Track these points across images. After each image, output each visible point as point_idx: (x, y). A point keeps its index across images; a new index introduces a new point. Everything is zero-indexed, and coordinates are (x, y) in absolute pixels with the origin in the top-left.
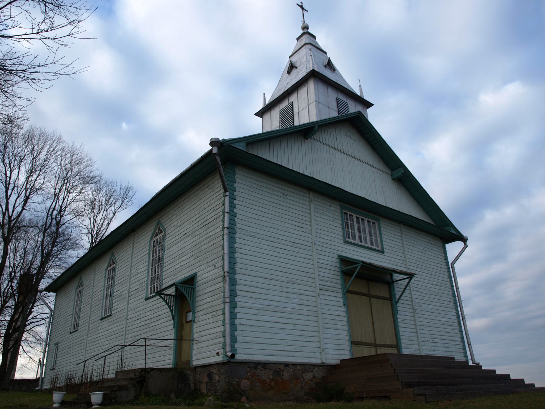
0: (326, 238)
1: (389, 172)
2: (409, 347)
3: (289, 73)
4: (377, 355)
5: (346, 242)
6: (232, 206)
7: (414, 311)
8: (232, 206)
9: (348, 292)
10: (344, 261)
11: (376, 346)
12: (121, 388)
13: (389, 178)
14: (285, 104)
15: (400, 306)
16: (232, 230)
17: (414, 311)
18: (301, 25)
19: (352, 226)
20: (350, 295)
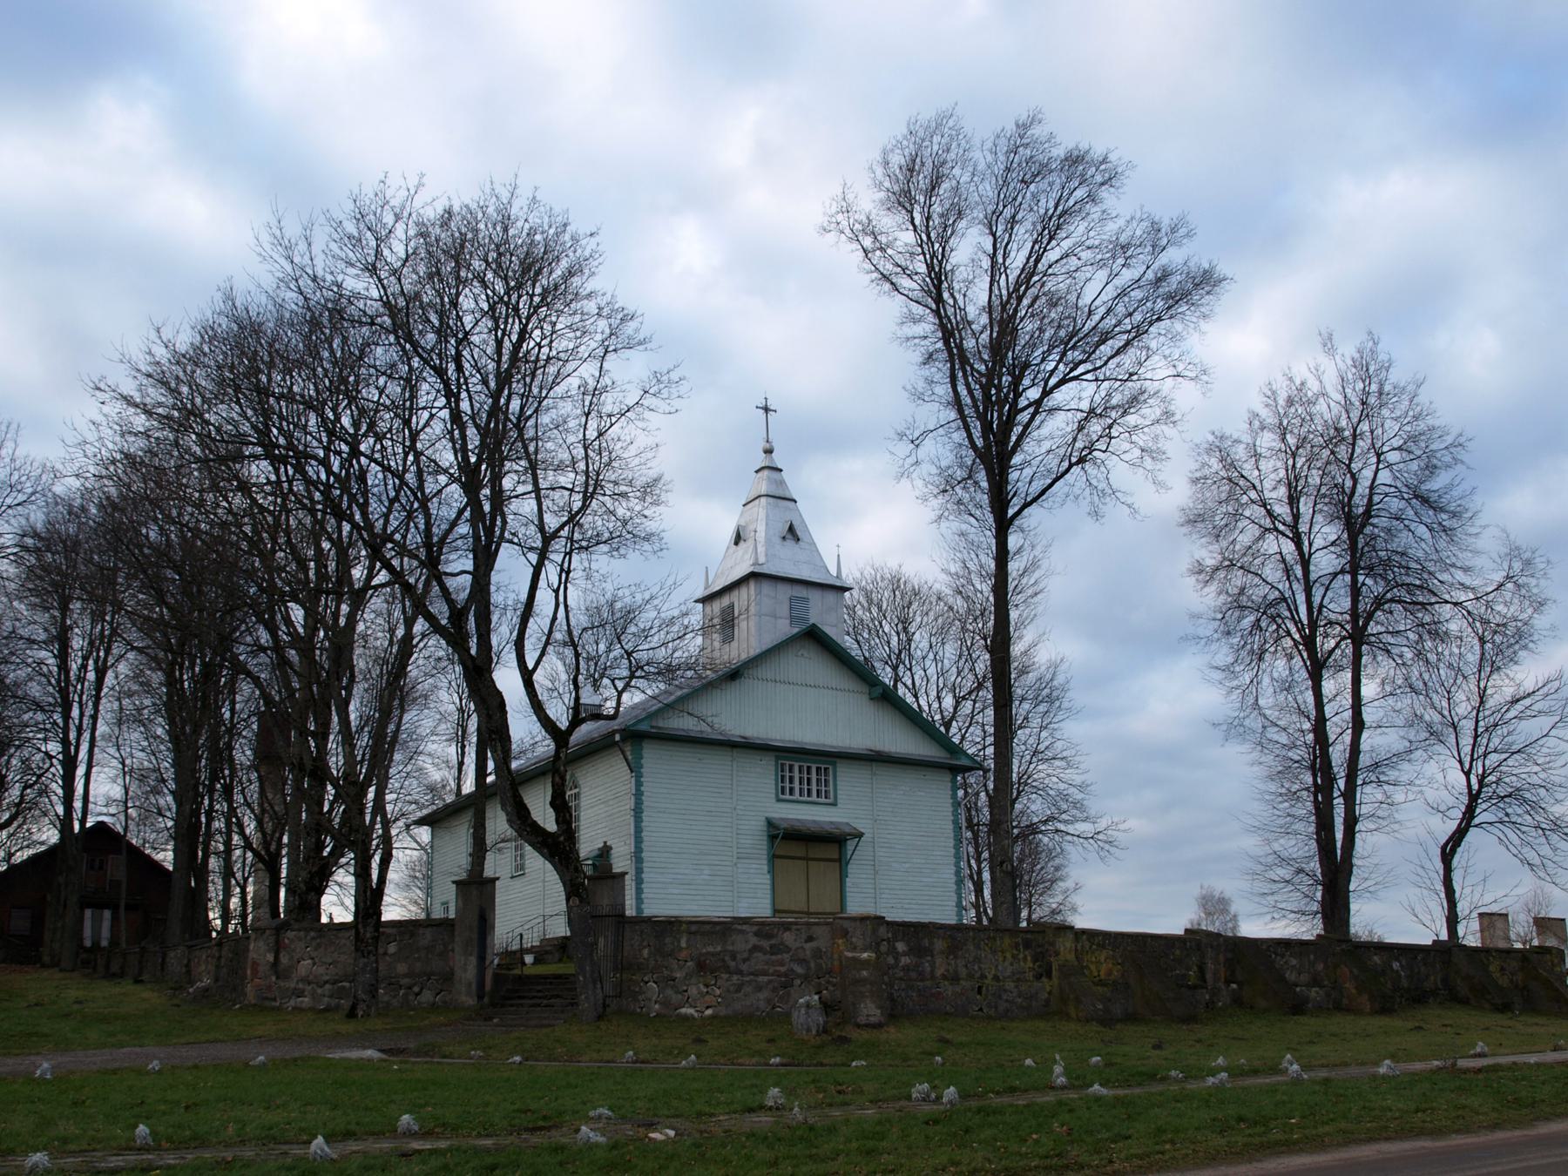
0: (757, 799)
1: (865, 689)
2: (1082, 921)
3: (736, 543)
4: (1339, 974)
5: (779, 800)
6: (639, 784)
7: (876, 873)
8: (639, 784)
9: (773, 858)
10: (770, 823)
11: (808, 913)
12: (547, 952)
13: (865, 698)
14: (726, 601)
15: (852, 869)
16: (638, 812)
17: (876, 873)
18: (763, 444)
19: (791, 780)
20: (778, 861)
